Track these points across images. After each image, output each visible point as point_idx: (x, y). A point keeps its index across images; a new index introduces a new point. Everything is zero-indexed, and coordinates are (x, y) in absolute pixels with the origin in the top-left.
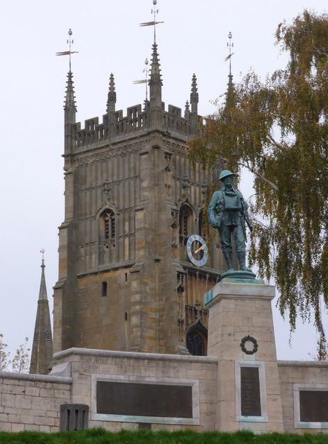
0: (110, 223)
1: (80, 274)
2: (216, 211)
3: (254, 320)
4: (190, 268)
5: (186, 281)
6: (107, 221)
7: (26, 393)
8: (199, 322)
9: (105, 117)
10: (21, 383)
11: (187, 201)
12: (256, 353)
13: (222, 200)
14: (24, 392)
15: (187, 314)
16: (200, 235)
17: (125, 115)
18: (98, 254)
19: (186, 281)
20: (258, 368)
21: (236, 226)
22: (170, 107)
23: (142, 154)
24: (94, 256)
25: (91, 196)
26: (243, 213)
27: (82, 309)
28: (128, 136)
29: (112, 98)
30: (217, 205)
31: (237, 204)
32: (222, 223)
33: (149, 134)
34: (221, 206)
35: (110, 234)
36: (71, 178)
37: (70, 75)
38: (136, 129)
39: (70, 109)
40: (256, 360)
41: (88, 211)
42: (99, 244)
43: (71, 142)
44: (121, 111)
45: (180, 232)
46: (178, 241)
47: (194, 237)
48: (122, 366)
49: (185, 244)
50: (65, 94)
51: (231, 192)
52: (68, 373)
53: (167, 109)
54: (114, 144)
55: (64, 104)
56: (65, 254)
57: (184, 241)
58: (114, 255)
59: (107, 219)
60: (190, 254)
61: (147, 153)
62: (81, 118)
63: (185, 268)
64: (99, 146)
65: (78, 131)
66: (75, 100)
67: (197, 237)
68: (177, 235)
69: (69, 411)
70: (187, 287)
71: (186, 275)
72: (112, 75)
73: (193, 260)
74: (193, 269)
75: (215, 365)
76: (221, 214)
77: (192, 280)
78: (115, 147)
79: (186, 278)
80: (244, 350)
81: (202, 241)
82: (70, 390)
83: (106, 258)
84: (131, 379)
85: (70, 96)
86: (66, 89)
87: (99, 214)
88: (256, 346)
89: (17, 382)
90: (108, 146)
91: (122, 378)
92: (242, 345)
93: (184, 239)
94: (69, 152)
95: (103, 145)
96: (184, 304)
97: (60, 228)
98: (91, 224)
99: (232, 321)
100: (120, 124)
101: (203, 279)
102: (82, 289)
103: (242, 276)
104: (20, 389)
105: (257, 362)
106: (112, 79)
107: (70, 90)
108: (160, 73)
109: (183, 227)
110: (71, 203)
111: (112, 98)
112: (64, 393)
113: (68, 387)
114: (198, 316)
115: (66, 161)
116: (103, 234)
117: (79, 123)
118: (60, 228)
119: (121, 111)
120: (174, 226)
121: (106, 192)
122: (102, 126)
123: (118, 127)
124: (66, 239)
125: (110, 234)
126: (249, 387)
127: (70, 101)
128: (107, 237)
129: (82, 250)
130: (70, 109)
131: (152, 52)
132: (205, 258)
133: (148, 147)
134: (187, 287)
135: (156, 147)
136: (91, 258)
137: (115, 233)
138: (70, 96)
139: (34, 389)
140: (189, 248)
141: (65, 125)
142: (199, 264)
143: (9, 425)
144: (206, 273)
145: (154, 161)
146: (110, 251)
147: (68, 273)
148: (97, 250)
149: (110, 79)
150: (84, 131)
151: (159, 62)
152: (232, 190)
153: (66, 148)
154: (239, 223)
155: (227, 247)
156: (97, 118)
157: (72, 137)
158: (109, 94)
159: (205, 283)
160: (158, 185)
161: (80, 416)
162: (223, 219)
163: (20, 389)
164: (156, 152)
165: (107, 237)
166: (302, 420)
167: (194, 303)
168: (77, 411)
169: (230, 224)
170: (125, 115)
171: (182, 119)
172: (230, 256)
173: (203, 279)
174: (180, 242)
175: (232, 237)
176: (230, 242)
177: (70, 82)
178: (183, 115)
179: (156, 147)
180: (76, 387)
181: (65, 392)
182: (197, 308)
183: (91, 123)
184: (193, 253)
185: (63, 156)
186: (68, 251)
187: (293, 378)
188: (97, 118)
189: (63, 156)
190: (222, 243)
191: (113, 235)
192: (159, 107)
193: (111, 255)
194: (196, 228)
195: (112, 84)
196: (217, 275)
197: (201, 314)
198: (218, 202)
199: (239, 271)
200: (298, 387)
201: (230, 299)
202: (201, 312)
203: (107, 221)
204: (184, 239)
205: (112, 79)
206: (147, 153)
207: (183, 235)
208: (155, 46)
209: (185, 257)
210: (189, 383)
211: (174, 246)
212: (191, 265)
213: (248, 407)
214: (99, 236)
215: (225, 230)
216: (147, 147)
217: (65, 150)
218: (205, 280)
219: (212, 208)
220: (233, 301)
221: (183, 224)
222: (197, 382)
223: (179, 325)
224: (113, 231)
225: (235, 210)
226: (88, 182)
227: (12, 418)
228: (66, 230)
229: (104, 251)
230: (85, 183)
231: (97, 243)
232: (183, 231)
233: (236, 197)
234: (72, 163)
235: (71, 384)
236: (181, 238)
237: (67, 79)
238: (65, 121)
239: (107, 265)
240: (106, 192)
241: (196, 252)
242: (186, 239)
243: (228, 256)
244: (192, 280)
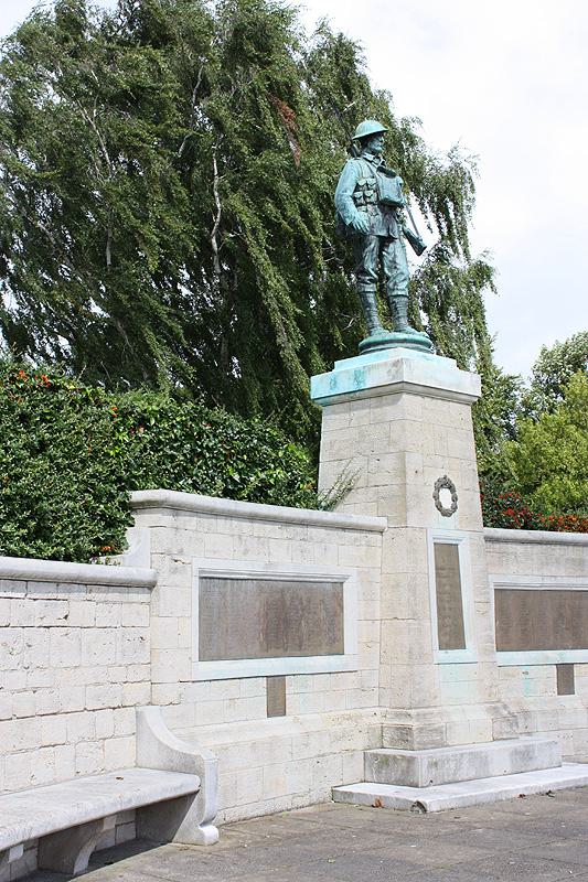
222: (353, 572)
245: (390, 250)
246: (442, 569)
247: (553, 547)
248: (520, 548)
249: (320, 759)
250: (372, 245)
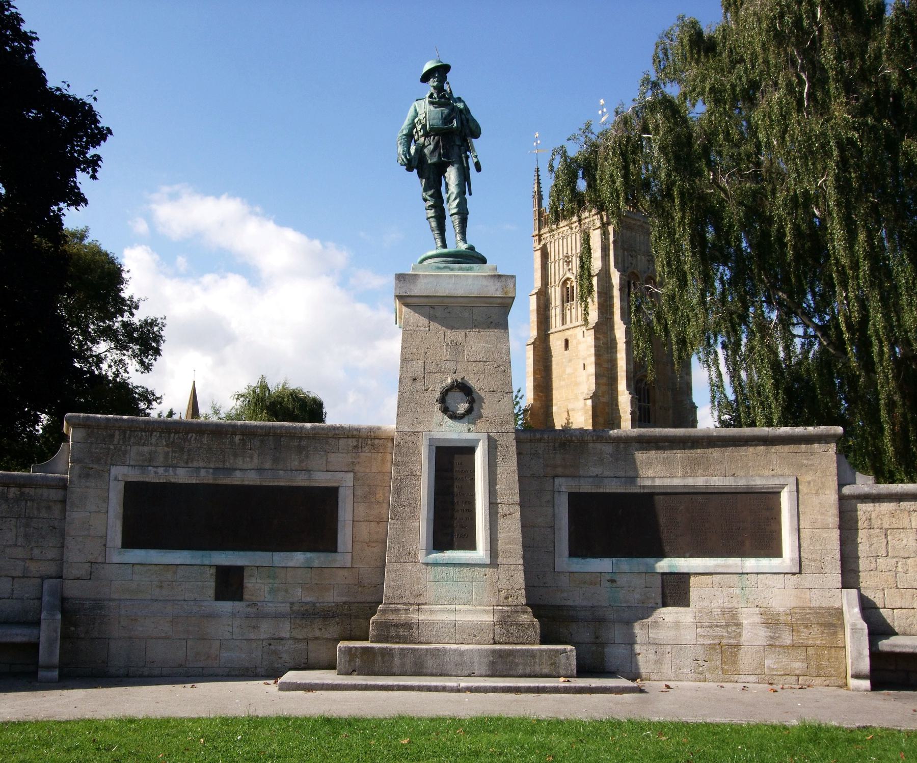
20: (437, 448)
166: (572, 554)
249: (272, 642)
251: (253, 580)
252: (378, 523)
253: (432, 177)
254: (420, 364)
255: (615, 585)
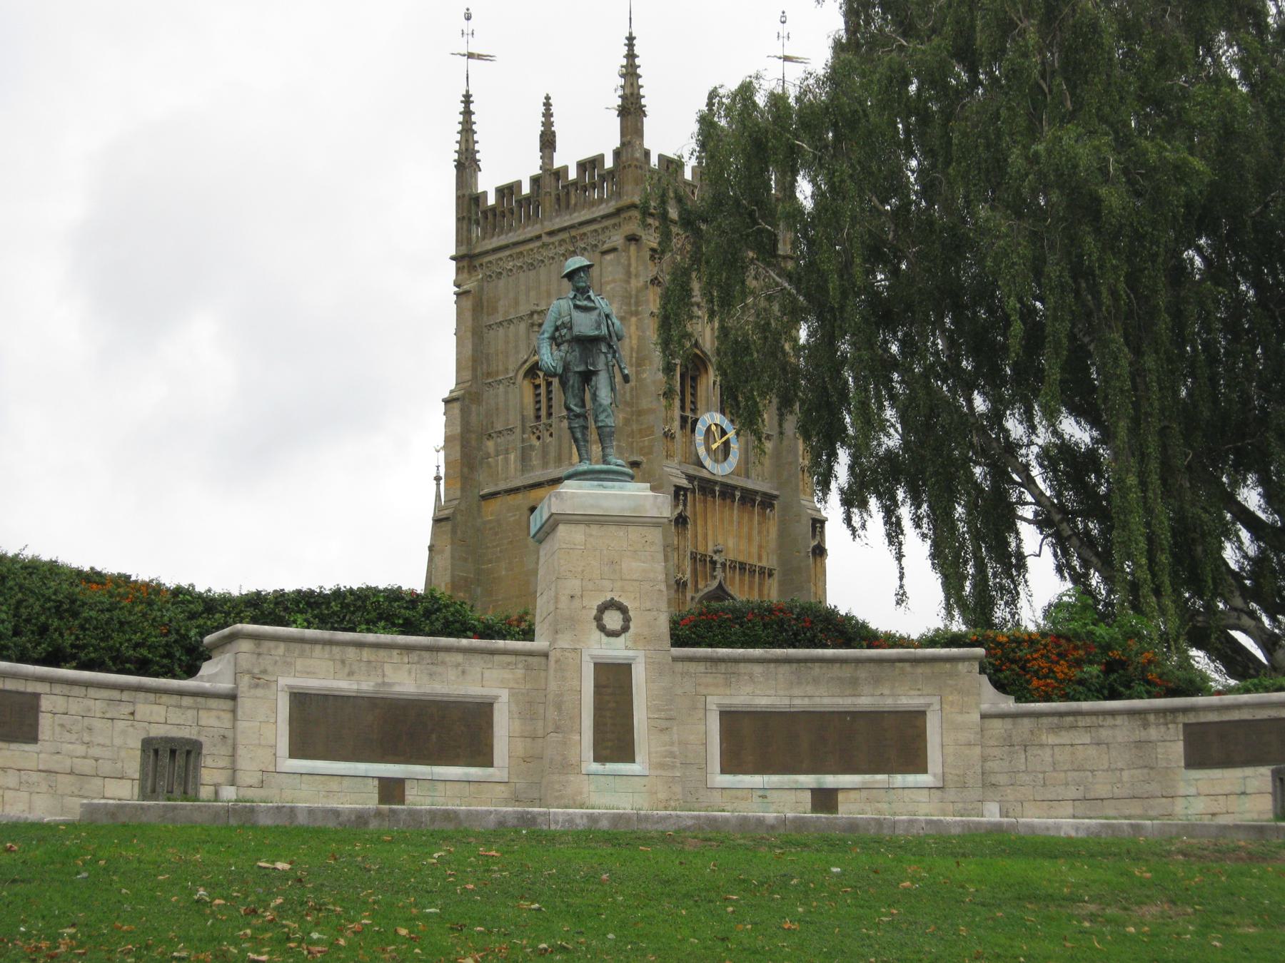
0: (543, 390)
1: (486, 491)
2: (555, 341)
3: (624, 566)
4: (702, 479)
5: (694, 505)
6: (537, 387)
7: (138, 717)
8: (720, 585)
9: (535, 181)
10: (126, 696)
11: (696, 345)
12: (627, 634)
13: (567, 319)
14: (132, 714)
15: (694, 571)
16: (723, 412)
17: (573, 175)
18: (519, 452)
19: (694, 505)
20: (630, 665)
21: (595, 373)
22: (661, 157)
23: (605, 253)
24: (512, 457)
25: (507, 336)
26: (610, 347)
27: (490, 561)
28: (584, 215)
29: (548, 142)
30: (557, 329)
31: (598, 327)
32: (566, 368)
33: (618, 212)
34: (564, 331)
35: (543, 413)
36: (468, 303)
37: (467, 100)
38: (593, 204)
39: (467, 164)
40: (627, 648)
41: (501, 368)
42: (523, 432)
43: (469, 231)
44: (565, 169)
45: (683, 408)
46: (677, 424)
47: (711, 418)
48: (343, 662)
49: (693, 430)
50: (458, 137)
51: (585, 303)
52: (229, 675)
53: (654, 161)
54: (551, 233)
55: (456, 156)
56: (457, 454)
57: (689, 424)
58: (552, 453)
59: (537, 382)
60: (702, 451)
61: (614, 250)
62: (488, 183)
63: (690, 478)
64: (522, 238)
65: (482, 207)
66: (477, 147)
67: (718, 418)
68: (677, 413)
69: (156, 752)
70: (695, 514)
71: (693, 491)
72: (548, 98)
73: (708, 462)
74: (709, 481)
75: (543, 660)
76: (564, 347)
77: (705, 502)
78: (552, 240)
79: (694, 500)
80: (602, 628)
81: (726, 424)
82: (234, 711)
83: (535, 462)
84: (797, 702)
85: (467, 141)
86: (460, 127)
87: (522, 373)
88: (627, 620)
89: (115, 694)
90: (539, 237)
91: (344, 685)
92: (598, 619)
93: (690, 421)
94: (464, 250)
95: (529, 236)
96: (690, 549)
97: (447, 402)
98: (506, 393)
99: (580, 569)
100: (562, 195)
101: (728, 501)
102: (490, 521)
103: (602, 476)
104: (126, 709)
105: (630, 653)
106: (547, 105)
107: (467, 129)
108: (642, 93)
109: (688, 398)
110: (468, 351)
111: (548, 142)
112: (218, 718)
113: (228, 704)
114: (719, 573)
115: (459, 270)
116: (530, 412)
117: (485, 193)
118: (447, 402)
119: (565, 169)
120: (668, 394)
121: (536, 329)
122: (528, 198)
123: (558, 199)
124: (458, 422)
125: (543, 413)
126: (612, 705)
127: (467, 150)
128: (538, 418)
129: (490, 445)
130: (467, 164)
131: (625, 50)
132: (734, 458)
133: (617, 239)
134: (695, 514)
135: (632, 239)
136: (506, 460)
137: (553, 410)
138: (467, 141)
139: (156, 708)
140: (699, 438)
141: (458, 198)
142: (720, 470)
143: (98, 781)
144: (735, 488)
145: (629, 265)
146: (544, 447)
147: (463, 489)
148: (519, 445)
149: (544, 104)
150: (493, 209)
151: (639, 71)
152: (589, 298)
153: (459, 242)
154: (601, 365)
155: (578, 416)
156: (519, 184)
157: (470, 219)
158: (543, 135)
159: (753, 512)
160: (636, 313)
161: (180, 760)
162: (569, 357)
163: (126, 709)
164: (633, 248)
165: (538, 418)
167: (711, 548)
168: (173, 752)
169: (581, 368)
170: (573, 175)
171: (686, 183)
172: (583, 434)
173: (728, 501)
174: (683, 427)
175: (588, 396)
176: (583, 406)
177: (467, 113)
178: (688, 175)
179: (632, 239)
180: (245, 704)
181: (222, 714)
182: (716, 558)
183: (507, 191)
184: (708, 449)
185: (453, 258)
186: (463, 446)
187: (707, 686)
188: (519, 184)
189: (453, 258)
190: (568, 409)
191: (550, 415)
192: (637, 160)
193: (545, 453)
194: (716, 399)
195: (548, 114)
196: (756, 492)
197: (724, 571)
198: (559, 323)
199: (598, 467)
200: (715, 702)
201: (577, 522)
202: (724, 565)
203: (537, 387)
204: (690, 421)
205: (547, 105)
206: (614, 250)
207: (688, 414)
208: (631, 39)
209: (694, 458)
210: (482, 696)
211: (669, 436)
212: (705, 474)
213: (610, 744)
214: (523, 416)
215: (573, 380)
216: (614, 238)
217: (457, 246)
218: (733, 501)
219: (546, 335)
220: (582, 527)
221: (689, 390)
222: (504, 695)
223: (677, 591)
224: (550, 407)
225: (595, 340)
226: (501, 310)
227: (106, 767)
228: (457, 405)
229: (532, 447)
230: (494, 310)
231: (518, 431)
232: (688, 405)
233: (596, 312)
234: (469, 272)
235: (233, 697)
236: (684, 420)
237: (461, 107)
238: (457, 190)
239: (538, 475)
240: (536, 329)
241: (714, 446)
242: (695, 422)
243: (579, 435)
244: (705, 502)
245: (593, 383)
246: (605, 687)
247: (809, 664)
248: (758, 669)
250: (571, 382)
251: (414, 792)
252: (534, 738)
253: (576, 385)
254: (577, 583)
255: (765, 800)
